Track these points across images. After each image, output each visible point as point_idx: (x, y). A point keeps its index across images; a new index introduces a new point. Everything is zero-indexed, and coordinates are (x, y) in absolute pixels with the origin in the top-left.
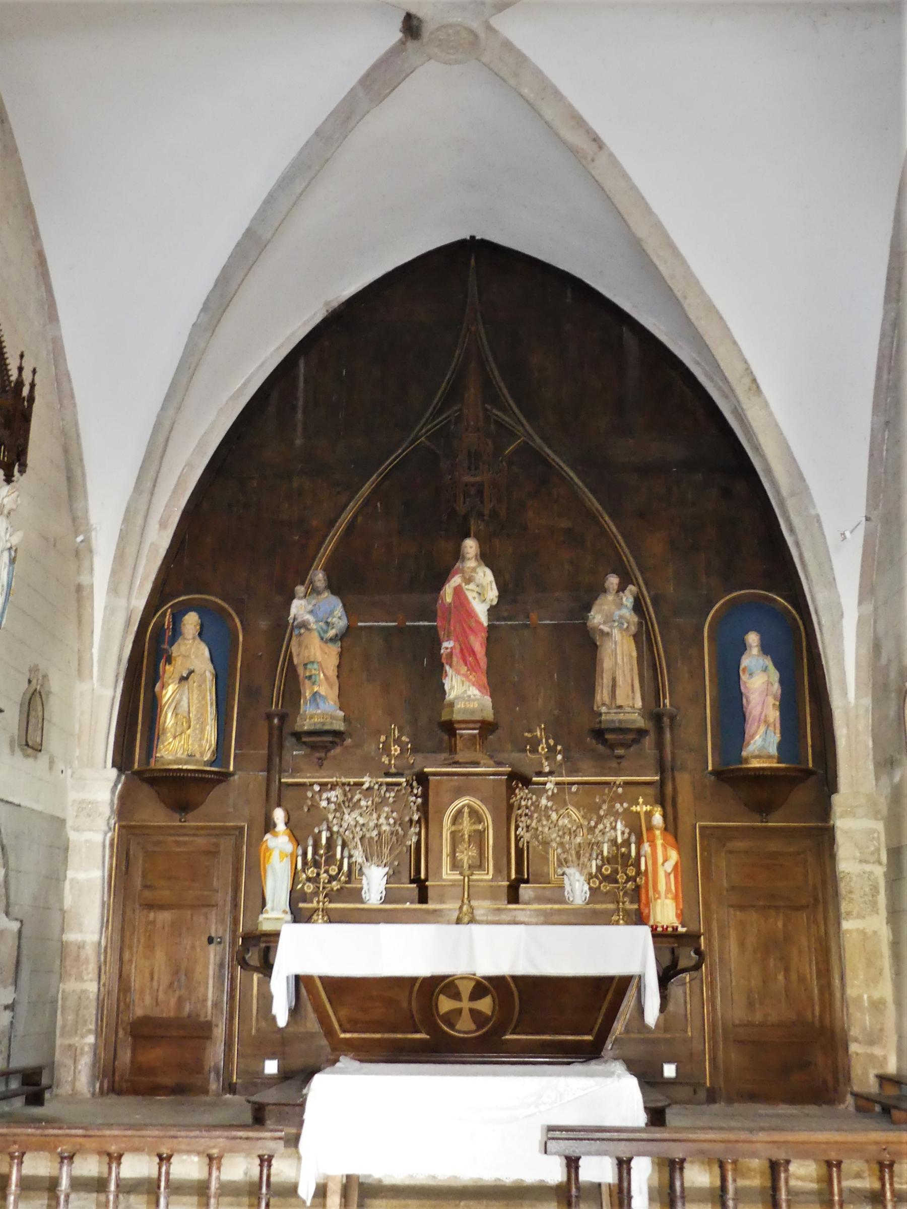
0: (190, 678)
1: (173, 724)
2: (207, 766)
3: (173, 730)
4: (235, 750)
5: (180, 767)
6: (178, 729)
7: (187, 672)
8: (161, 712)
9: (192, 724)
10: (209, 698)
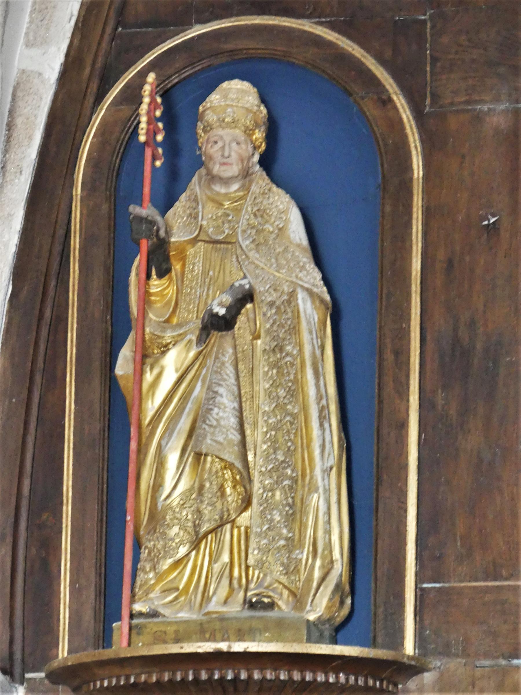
0: (241, 319)
1: (190, 490)
2: (320, 640)
3: (187, 514)
4: (419, 578)
5: (223, 646)
6: (207, 511)
7: (227, 299)
8: (142, 451)
9: (257, 488)
10: (312, 391)
